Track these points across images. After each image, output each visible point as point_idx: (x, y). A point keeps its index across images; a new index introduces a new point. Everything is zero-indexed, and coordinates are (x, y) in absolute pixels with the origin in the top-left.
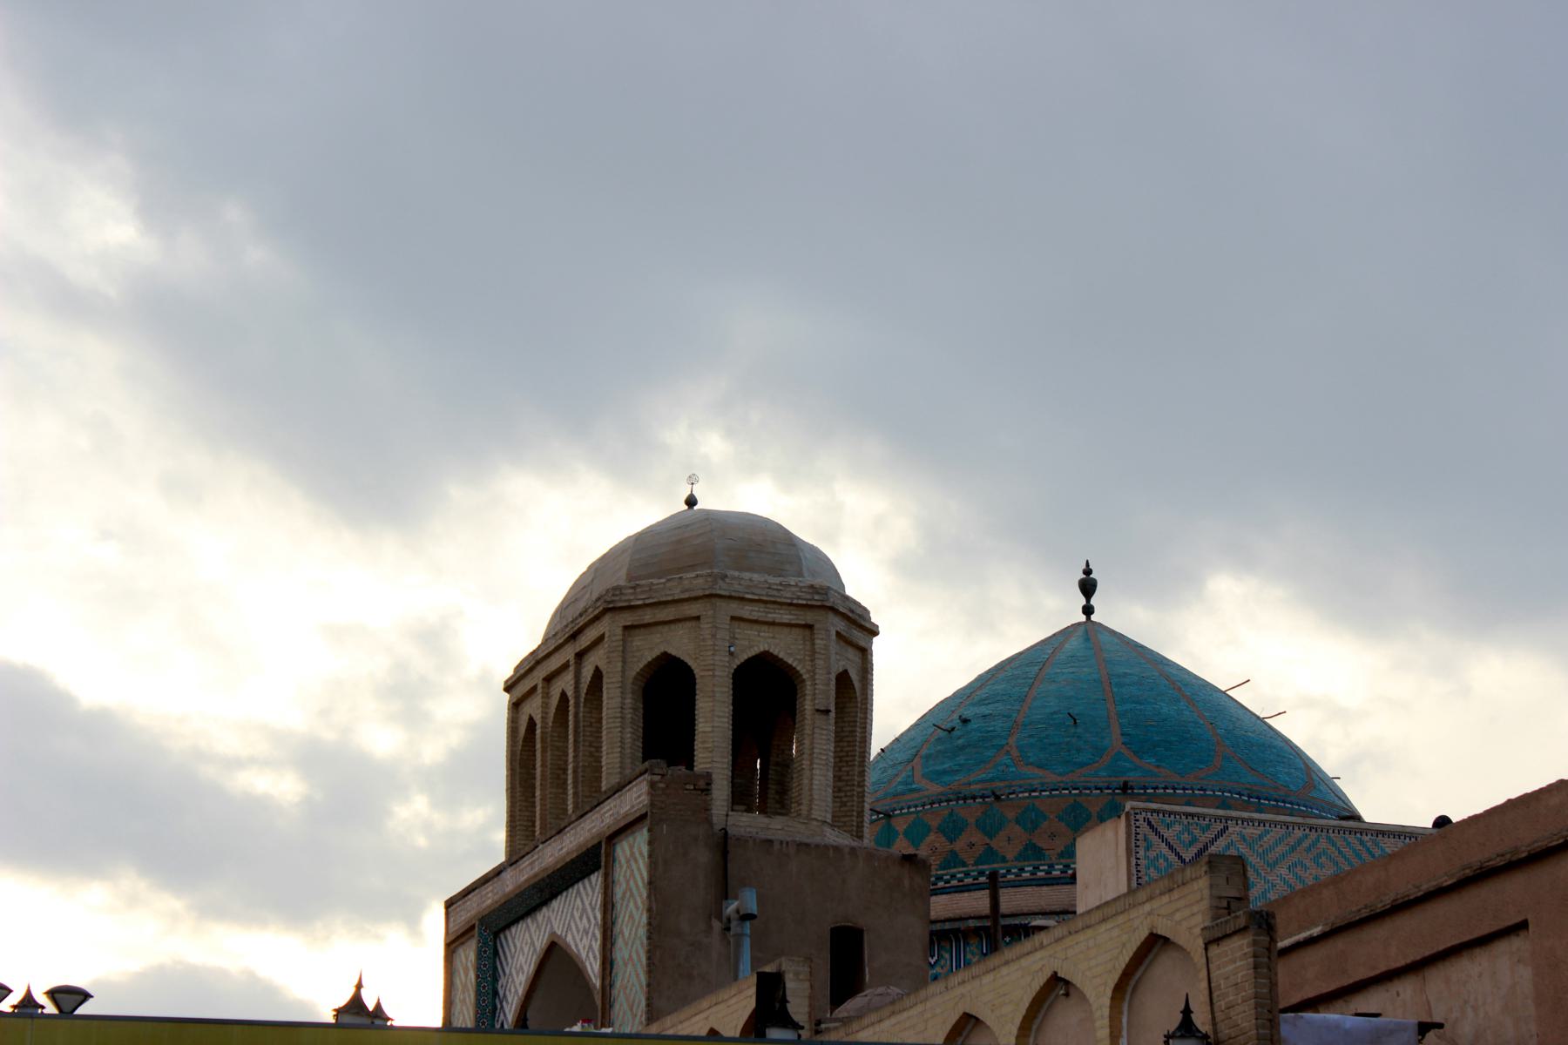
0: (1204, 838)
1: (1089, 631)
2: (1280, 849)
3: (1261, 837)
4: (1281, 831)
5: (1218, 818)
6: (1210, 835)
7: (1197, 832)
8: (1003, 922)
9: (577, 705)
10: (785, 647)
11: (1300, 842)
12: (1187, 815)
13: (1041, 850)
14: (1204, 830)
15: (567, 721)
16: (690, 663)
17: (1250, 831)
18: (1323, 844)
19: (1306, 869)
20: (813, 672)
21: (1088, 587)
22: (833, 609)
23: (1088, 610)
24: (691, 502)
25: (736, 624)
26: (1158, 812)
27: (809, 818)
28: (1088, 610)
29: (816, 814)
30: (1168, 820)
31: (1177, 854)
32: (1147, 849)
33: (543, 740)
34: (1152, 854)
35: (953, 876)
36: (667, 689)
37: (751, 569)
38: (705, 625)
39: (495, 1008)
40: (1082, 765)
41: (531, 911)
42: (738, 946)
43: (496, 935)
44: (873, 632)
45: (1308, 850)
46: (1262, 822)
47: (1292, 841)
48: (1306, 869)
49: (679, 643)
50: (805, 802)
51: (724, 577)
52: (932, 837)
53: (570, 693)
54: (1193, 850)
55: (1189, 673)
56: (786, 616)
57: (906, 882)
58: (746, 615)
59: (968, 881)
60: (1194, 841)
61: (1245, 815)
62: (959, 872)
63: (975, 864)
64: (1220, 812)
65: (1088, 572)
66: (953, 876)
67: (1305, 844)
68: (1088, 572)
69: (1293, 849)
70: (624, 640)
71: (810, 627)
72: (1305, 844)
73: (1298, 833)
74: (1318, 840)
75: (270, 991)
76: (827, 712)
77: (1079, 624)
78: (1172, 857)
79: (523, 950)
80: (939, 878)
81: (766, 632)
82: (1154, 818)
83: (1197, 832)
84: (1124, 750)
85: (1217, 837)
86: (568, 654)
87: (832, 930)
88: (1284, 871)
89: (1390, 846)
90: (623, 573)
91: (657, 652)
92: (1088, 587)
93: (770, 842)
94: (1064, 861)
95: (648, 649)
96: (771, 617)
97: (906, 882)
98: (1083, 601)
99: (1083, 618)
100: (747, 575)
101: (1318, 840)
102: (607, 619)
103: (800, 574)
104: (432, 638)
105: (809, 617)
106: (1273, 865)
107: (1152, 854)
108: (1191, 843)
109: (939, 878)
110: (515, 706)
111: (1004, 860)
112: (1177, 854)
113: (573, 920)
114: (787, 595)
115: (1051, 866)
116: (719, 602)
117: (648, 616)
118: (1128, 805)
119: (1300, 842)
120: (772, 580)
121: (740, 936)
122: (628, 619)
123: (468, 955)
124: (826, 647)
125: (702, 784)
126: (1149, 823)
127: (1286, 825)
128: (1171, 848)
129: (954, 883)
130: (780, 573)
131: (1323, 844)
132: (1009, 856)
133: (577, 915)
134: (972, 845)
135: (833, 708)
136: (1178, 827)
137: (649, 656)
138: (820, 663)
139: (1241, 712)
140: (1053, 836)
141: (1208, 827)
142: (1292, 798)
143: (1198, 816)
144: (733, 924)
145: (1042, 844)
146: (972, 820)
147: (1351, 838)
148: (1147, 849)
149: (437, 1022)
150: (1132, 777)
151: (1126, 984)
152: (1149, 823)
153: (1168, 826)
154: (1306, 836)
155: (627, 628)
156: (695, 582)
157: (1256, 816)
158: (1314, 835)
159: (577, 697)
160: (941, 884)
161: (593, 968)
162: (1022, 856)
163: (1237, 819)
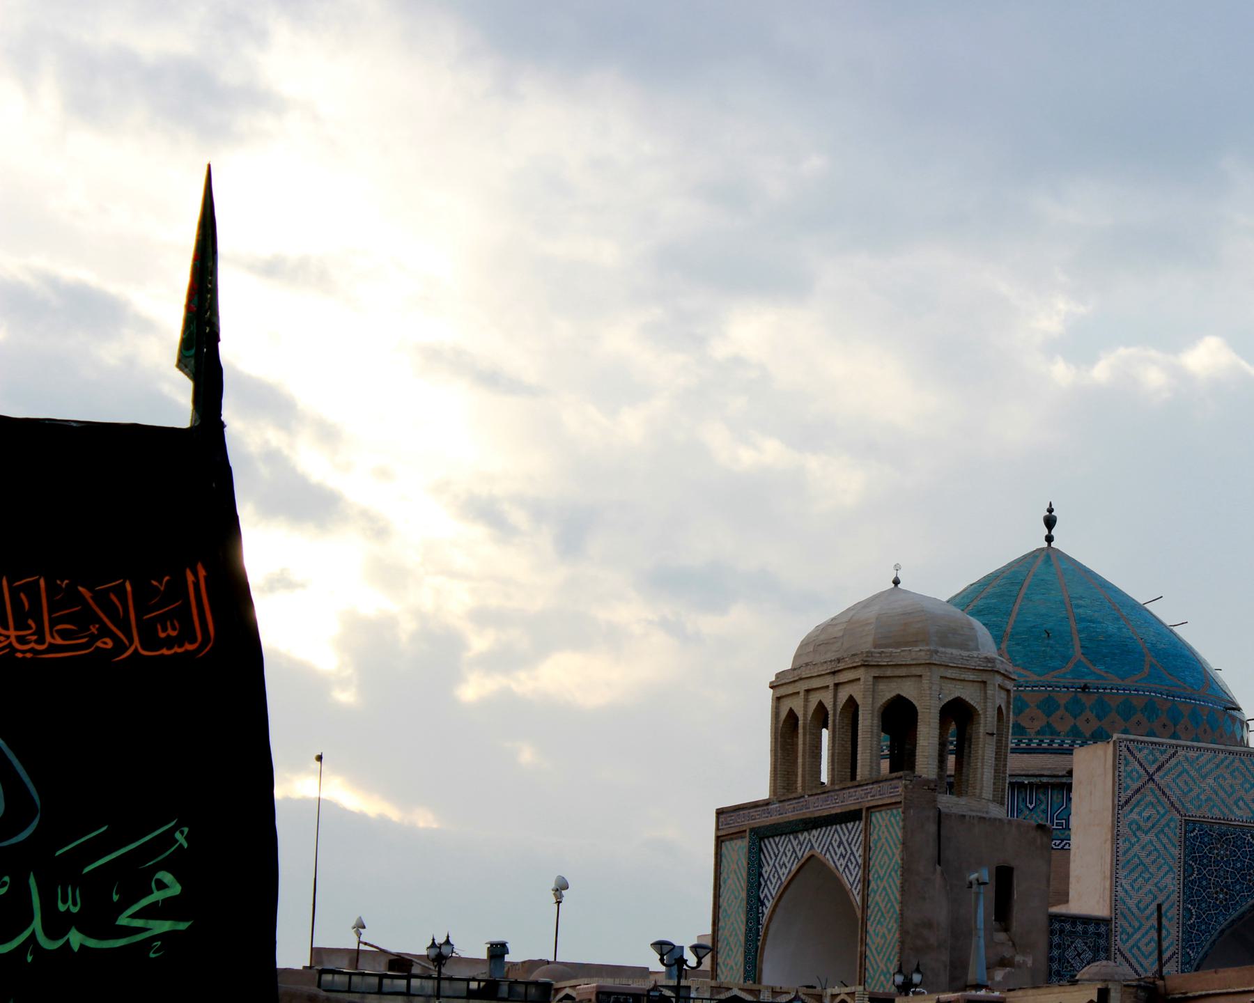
0: (1162, 758)
1: (1048, 556)
4: (1209, 755)
5: (1171, 746)
6: (1166, 756)
9: (834, 715)
10: (970, 695)
11: (1222, 761)
12: (1152, 743)
13: (1024, 728)
14: (1162, 753)
16: (918, 708)
18: (1237, 763)
19: (1225, 779)
20: (985, 710)
21: (1050, 522)
22: (998, 672)
23: (1049, 539)
24: (896, 582)
26: (1133, 741)
27: (980, 797)
28: (1049, 539)
29: (984, 795)
32: (1126, 765)
33: (804, 728)
34: (1129, 769)
36: (899, 718)
38: (925, 681)
39: (760, 884)
40: (1054, 669)
42: (977, 899)
43: (762, 839)
45: (1227, 767)
46: (1199, 749)
47: (1217, 761)
48: (1225, 779)
49: (908, 690)
50: (978, 787)
51: (936, 652)
53: (829, 707)
54: (1155, 766)
56: (972, 677)
57: (1039, 841)
58: (948, 675)
61: (1189, 743)
64: (1174, 742)
65: (1050, 510)
67: (1226, 763)
68: (1050, 510)
69: (1217, 766)
70: (874, 685)
71: (984, 682)
72: (1226, 763)
73: (1222, 756)
76: (992, 734)
77: (1042, 549)
78: (1142, 771)
79: (783, 859)
81: (959, 685)
82: (1131, 746)
83: (1158, 754)
84: (1083, 659)
86: (829, 681)
88: (1211, 781)
90: (870, 639)
91: (893, 694)
92: (1050, 522)
93: (964, 816)
94: (1040, 737)
95: (888, 692)
96: (963, 677)
97: (1039, 841)
98: (1046, 532)
99: (1045, 544)
100: (949, 650)
102: (862, 670)
103: (977, 649)
105: (984, 677)
106: (1204, 777)
107: (1129, 769)
108: (1154, 762)
110: (778, 700)
113: (836, 849)
114: (972, 664)
115: (1030, 740)
116: (934, 668)
117: (889, 673)
118: (1115, 736)
119: (1222, 761)
120: (965, 654)
121: (978, 894)
122: (876, 672)
123: (738, 850)
124: (993, 695)
127: (1214, 750)
128: (1141, 765)
130: (963, 646)
131: (1237, 763)
133: (835, 845)
136: (1146, 751)
138: (989, 704)
140: (1032, 719)
142: (1196, 696)
143: (1159, 744)
144: (974, 887)
145: (1023, 724)
148: (1126, 765)
150: (1089, 680)
153: (1140, 750)
156: (918, 653)
157: (1195, 744)
158: (1231, 757)
159: (835, 710)
161: (850, 878)
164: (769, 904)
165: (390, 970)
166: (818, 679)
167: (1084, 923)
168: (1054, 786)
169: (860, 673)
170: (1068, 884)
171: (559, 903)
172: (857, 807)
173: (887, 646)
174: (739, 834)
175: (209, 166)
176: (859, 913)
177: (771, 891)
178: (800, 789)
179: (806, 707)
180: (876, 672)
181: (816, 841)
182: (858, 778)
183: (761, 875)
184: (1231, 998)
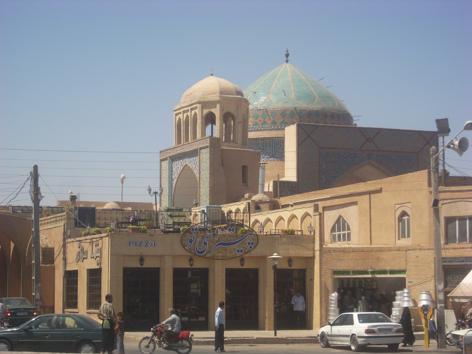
8: (212, 334)
15: (188, 137)
25: (372, 243)
35: (262, 127)
41: (293, 343)
53: (182, 119)
55: (17, 351)
59: (259, 129)
62: (257, 126)
63: (261, 125)
75: (329, 98)
80: (253, 128)
87: (449, 130)
89: (282, 144)
95: (206, 111)
104: (232, 111)
109: (253, 128)
111: (267, 124)
122: (181, 214)
123: (165, 164)
125: (282, 185)
132: (269, 123)
134: (260, 121)
135: (371, 246)
146: (260, 115)
149: (277, 331)
151: (303, 219)
155: (78, 312)
161: (196, 172)
162: (281, 123)
164: (175, 180)
165: (43, 251)
166: (450, 194)
167: (256, 140)
168: (371, 242)
169: (198, 105)
170: (174, 291)
171: (122, 183)
172: (197, 148)
173: (206, 95)
174: (166, 159)
175: (36, 168)
176: (198, 179)
177: (175, 176)
178: (190, 140)
179: (183, 116)
180: (181, 214)
181: (187, 161)
182: (198, 138)
183: (172, 171)
184: (369, 201)
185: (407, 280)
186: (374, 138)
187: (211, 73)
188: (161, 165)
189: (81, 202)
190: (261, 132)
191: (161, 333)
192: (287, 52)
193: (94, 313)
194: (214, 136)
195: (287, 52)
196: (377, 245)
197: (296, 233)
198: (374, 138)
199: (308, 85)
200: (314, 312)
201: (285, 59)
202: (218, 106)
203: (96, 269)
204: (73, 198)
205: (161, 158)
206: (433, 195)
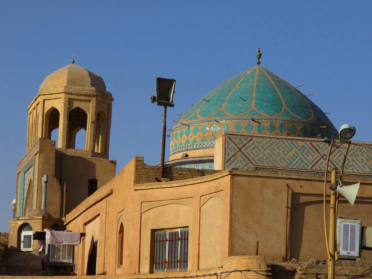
0: (245, 142)
2: (268, 144)
3: (262, 141)
4: (268, 140)
6: (247, 141)
7: (243, 140)
17: (259, 140)
18: (281, 143)
30: (235, 137)
31: (237, 146)
35: (204, 144)
37: (76, 85)
44: (113, 100)
48: (275, 150)
52: (199, 133)
56: (83, 98)
60: (242, 142)
66: (204, 144)
67: (276, 143)
69: (271, 145)
72: (276, 143)
74: (279, 142)
78: (235, 147)
85: (249, 141)
91: (51, 107)
97: (110, 167)
101: (279, 142)
109: (200, 144)
112: (237, 146)
114: (83, 93)
125: (53, 144)
126: (229, 138)
127: (270, 138)
128: (235, 145)
129: (204, 146)
136: (238, 139)
137: (49, 107)
139: (40, 168)
141: (247, 139)
147: (289, 142)
149: (370, 187)
152: (229, 138)
153: (235, 139)
154: (276, 141)
158: (278, 141)
160: (201, 146)
163: (255, 136)
185: (95, 276)
186: (69, 222)
187: (72, 61)
188: (200, 199)
189: (63, 147)
190: (210, 149)
191: (225, 258)
192: (259, 51)
193: (172, 161)
194: (75, 102)
195: (259, 51)
196: (82, 210)
197: (43, 178)
198: (69, 222)
199: (276, 92)
200: (330, 215)
201: (257, 60)
202: (45, 230)
203: (40, 84)
204: (154, 100)
205: (330, 174)
206: (329, 265)
